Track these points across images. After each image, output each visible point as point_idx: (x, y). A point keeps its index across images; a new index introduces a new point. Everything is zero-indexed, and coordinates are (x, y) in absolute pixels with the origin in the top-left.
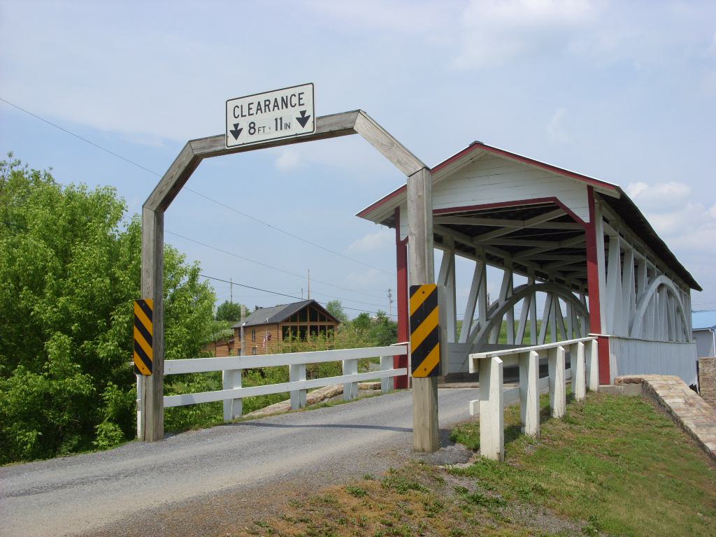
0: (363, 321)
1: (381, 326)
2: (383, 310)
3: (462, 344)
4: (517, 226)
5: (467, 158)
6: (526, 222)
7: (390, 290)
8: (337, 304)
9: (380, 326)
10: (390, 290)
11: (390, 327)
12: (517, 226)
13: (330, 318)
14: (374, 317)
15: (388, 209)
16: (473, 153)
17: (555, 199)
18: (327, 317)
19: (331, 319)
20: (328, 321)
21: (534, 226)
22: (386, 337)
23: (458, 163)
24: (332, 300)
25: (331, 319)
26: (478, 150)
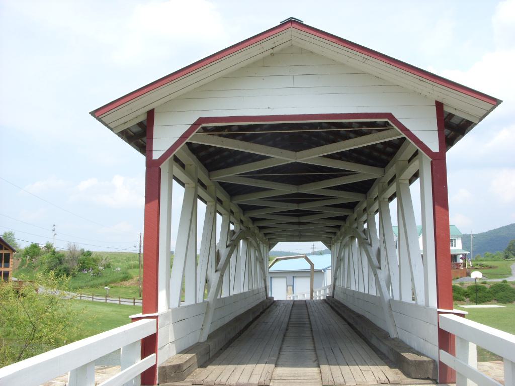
0: (34, 251)
1: (49, 255)
2: (51, 241)
3: (201, 303)
4: (281, 157)
5: (267, 44)
6: (299, 154)
7: (54, 226)
8: (11, 234)
9: (48, 254)
10: (54, 226)
11: (57, 256)
12: (281, 157)
13: (6, 247)
14: (42, 246)
15: (134, 115)
16: (278, 38)
17: (389, 116)
18: (4, 246)
19: (8, 248)
20: (6, 249)
21: (305, 160)
22: (54, 264)
23: (254, 51)
24: (7, 231)
25: (8, 248)
26: (292, 32)
